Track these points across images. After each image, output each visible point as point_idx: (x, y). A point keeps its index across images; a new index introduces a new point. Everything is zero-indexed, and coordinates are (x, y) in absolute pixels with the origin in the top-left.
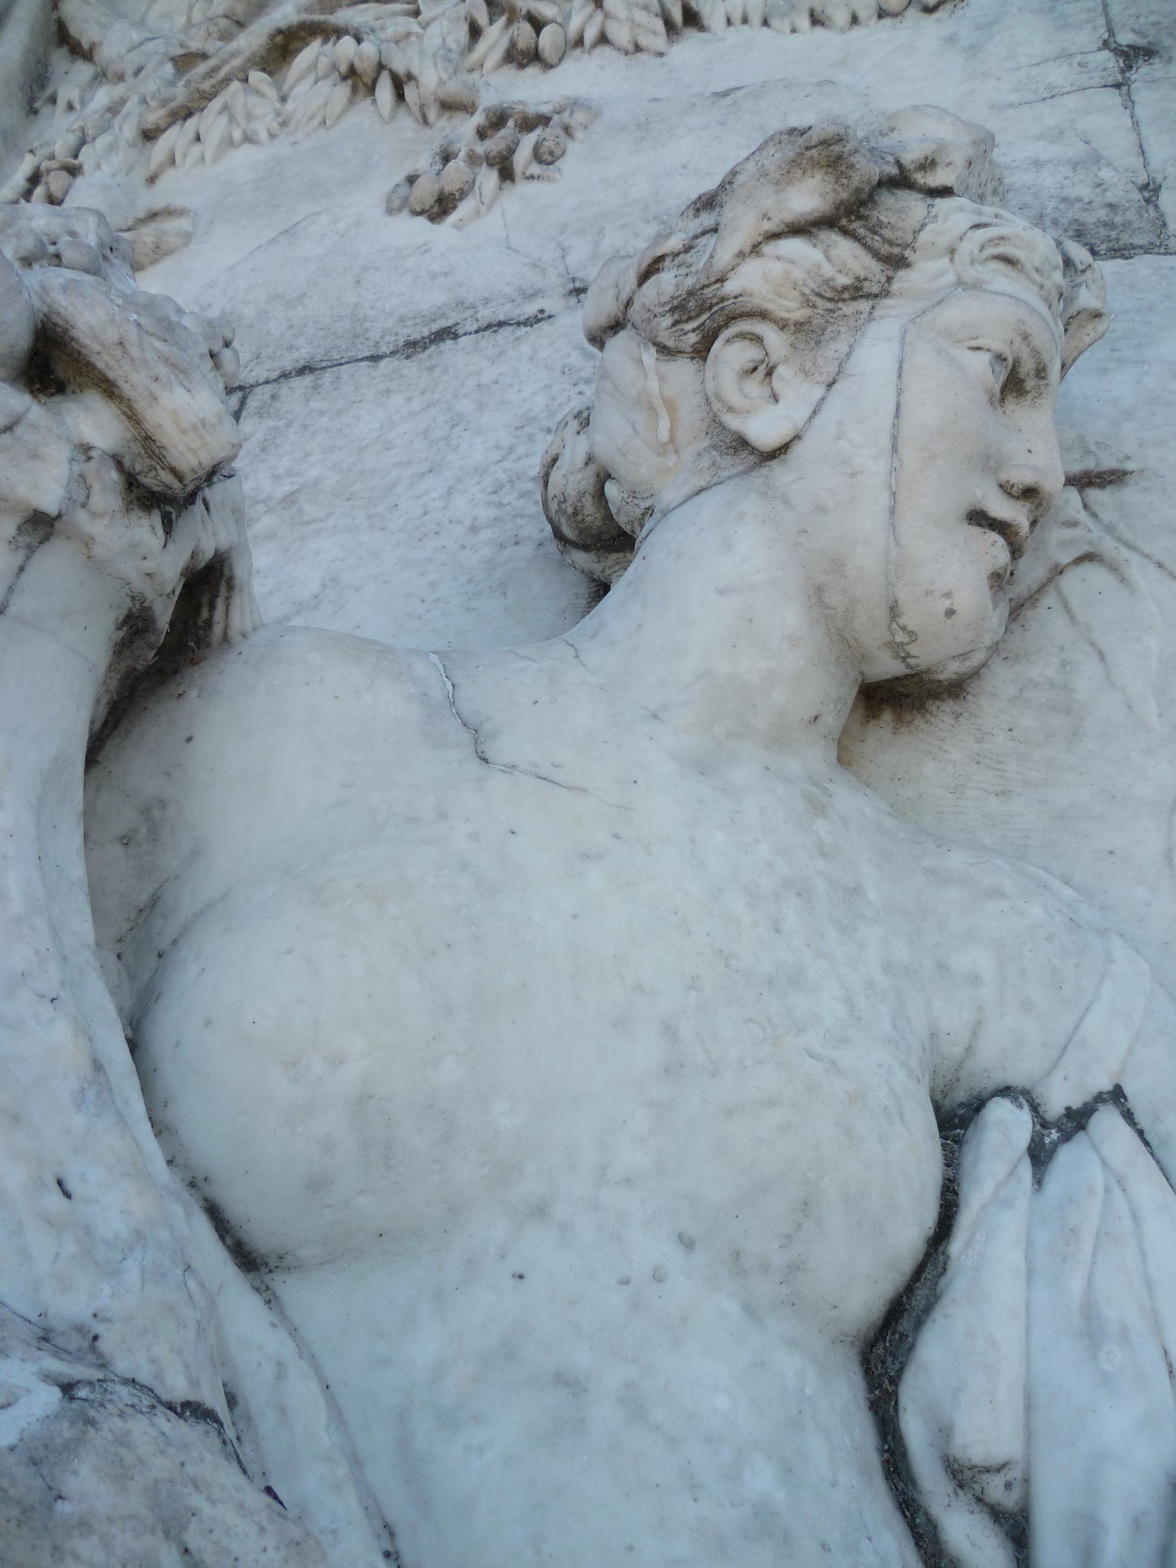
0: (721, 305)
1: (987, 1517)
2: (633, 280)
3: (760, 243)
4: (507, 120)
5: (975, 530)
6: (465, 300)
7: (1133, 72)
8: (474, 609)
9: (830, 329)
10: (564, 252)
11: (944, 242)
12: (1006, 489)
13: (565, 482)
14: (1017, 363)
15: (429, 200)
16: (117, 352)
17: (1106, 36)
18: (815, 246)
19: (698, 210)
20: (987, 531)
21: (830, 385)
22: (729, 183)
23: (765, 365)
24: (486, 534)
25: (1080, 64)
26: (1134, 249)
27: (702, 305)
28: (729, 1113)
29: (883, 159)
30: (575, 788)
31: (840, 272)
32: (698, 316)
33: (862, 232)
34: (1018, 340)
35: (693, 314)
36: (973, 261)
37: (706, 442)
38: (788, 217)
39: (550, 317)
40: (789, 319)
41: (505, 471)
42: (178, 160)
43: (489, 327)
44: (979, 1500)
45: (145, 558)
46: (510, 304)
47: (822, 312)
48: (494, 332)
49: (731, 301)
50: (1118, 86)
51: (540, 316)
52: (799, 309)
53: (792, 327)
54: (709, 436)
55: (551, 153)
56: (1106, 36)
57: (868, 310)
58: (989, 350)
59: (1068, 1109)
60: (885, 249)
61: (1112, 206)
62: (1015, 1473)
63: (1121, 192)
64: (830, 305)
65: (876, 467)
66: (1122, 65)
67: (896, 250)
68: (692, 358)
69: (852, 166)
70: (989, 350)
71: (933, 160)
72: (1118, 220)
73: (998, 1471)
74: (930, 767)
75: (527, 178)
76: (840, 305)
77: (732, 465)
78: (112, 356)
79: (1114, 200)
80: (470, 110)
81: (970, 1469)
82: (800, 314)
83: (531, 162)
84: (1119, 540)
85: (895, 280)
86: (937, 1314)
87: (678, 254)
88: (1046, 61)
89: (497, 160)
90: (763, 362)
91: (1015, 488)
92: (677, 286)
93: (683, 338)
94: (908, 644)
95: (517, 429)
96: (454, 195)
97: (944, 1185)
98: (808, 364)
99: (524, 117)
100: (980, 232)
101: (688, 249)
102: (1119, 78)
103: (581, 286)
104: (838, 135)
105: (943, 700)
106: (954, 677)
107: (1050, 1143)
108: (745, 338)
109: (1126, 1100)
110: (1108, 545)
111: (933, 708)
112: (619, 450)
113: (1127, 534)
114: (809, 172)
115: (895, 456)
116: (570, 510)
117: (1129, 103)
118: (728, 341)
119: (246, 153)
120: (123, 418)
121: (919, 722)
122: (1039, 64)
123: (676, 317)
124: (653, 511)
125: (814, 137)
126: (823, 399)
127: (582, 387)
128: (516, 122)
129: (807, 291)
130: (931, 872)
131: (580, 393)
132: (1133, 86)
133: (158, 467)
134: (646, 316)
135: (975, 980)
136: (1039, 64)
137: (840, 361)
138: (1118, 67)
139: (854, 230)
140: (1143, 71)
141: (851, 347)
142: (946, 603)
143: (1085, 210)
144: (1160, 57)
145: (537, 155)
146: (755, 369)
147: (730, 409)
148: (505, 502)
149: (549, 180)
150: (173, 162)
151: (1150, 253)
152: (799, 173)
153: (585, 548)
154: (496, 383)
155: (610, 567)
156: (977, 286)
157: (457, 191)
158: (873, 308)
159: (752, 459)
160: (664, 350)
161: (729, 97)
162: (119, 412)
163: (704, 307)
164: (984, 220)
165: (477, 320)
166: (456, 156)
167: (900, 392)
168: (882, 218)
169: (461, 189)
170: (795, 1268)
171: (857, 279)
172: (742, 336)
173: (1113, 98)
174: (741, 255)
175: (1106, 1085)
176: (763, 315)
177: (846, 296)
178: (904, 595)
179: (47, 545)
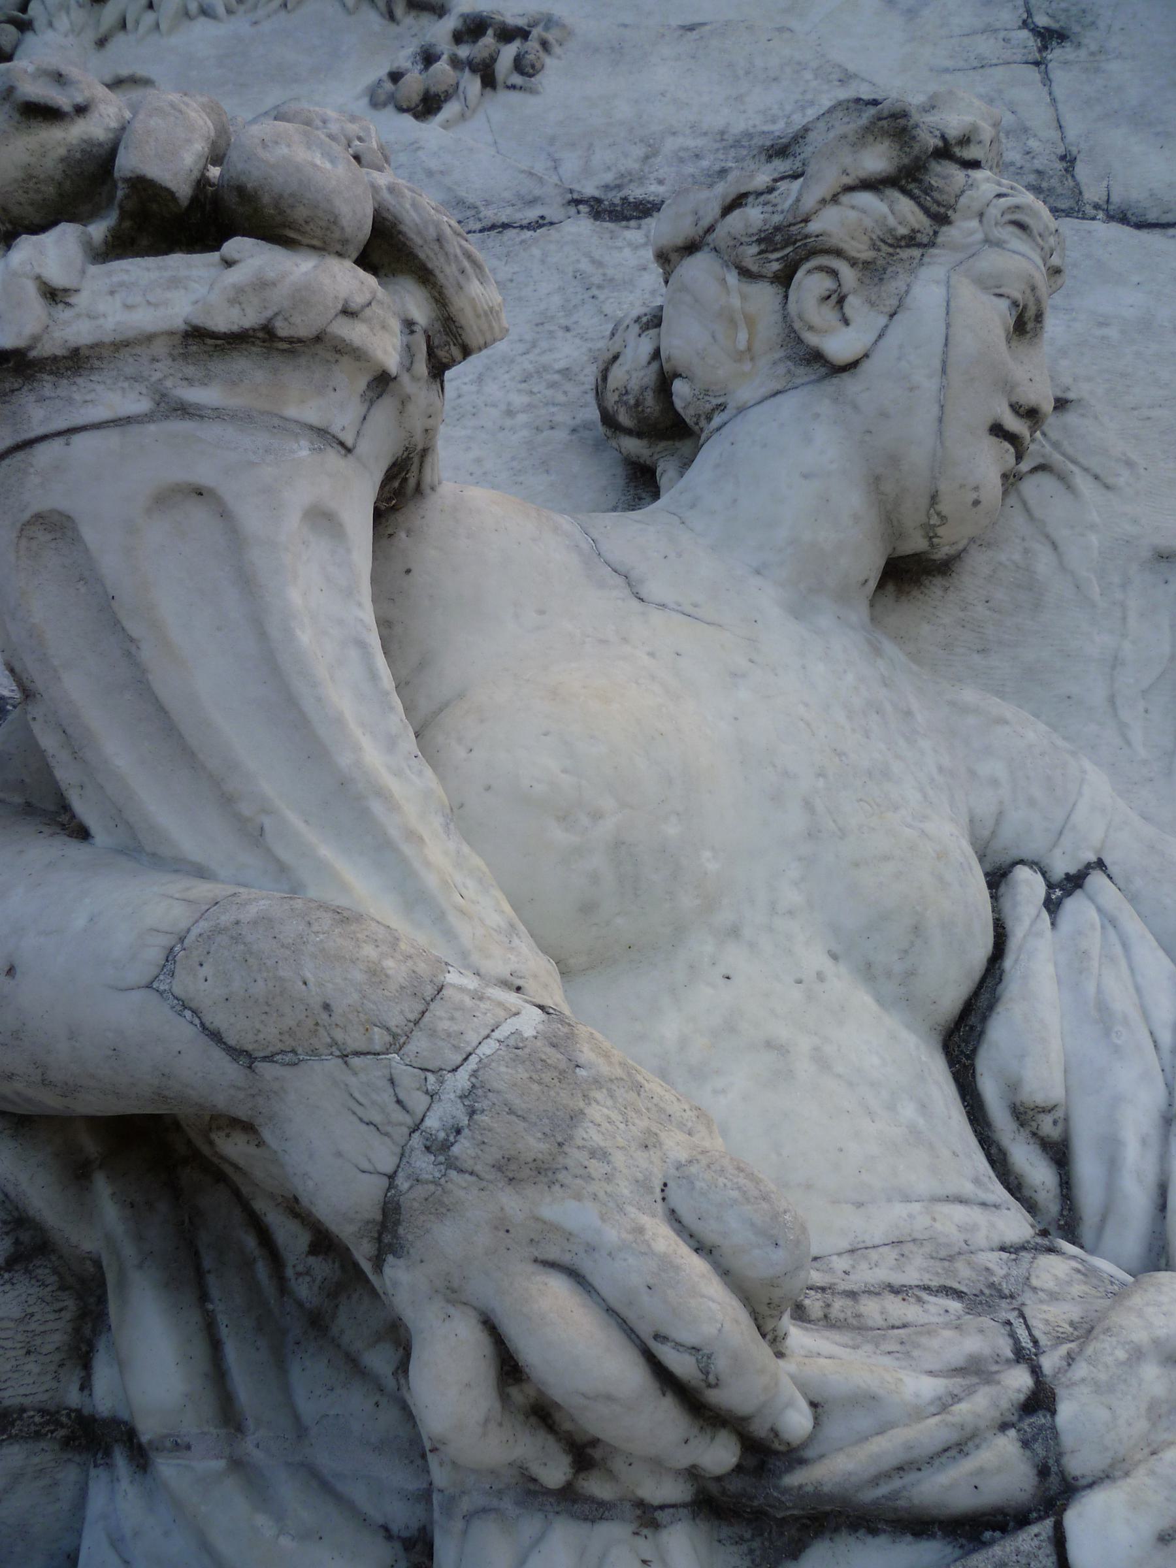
0: (805, 241)
1: (1038, 1147)
2: (717, 211)
3: (838, 194)
4: (487, 30)
5: (994, 439)
6: (465, 200)
7: (1049, 51)
8: (521, 483)
9: (890, 270)
10: (556, 165)
11: (976, 206)
12: (1015, 408)
13: (628, 377)
14: (1025, 307)
15: (416, 98)
16: (435, 247)
17: (1025, 16)
18: (882, 200)
19: (770, 157)
20: (1003, 441)
21: (892, 316)
22: (801, 137)
23: (837, 294)
24: (522, 418)
25: (1004, 40)
26: (1057, 212)
27: (788, 239)
28: (857, 865)
29: (931, 132)
30: (713, 624)
31: (900, 223)
32: (782, 248)
33: (916, 191)
34: (1028, 291)
35: (779, 246)
36: (996, 224)
37: (780, 354)
38: (862, 174)
39: (552, 224)
40: (859, 259)
41: (531, 362)
42: (129, 25)
43: (493, 227)
44: (1034, 1134)
45: (430, 416)
46: (511, 208)
47: (884, 255)
48: (499, 232)
49: (813, 239)
50: (1037, 64)
51: (541, 221)
52: (867, 250)
53: (861, 265)
54: (783, 348)
55: (533, 66)
56: (1025, 16)
57: (919, 255)
58: (1008, 297)
59: (1067, 874)
60: (934, 208)
61: (1039, 172)
62: (1059, 1114)
63: (1046, 162)
64: (891, 250)
65: (929, 385)
66: (1039, 45)
67: (942, 210)
68: (772, 283)
69: (914, 138)
70: (1008, 297)
71: (969, 137)
72: (1044, 185)
73: (1049, 1111)
74: (925, 628)
75: (508, 87)
76: (898, 250)
77: (803, 373)
78: (432, 249)
79: (1041, 168)
80: (438, 11)
81: (1032, 1110)
82: (868, 255)
83: (512, 73)
84: (1064, 454)
85: (940, 234)
86: (1000, 1008)
87: (761, 194)
88: (975, 33)
89: (481, 67)
90: (836, 291)
91: (1022, 409)
92: (765, 221)
93: (767, 265)
94: (939, 526)
95: (537, 325)
96: (440, 97)
97: (994, 923)
98: (874, 298)
99: (504, 28)
100: (1002, 200)
101: (771, 190)
102: (1038, 56)
103: (579, 198)
104: (904, 111)
105: (934, 576)
106: (945, 557)
107: (1056, 898)
108: (822, 271)
109: (1106, 869)
110: (1057, 458)
111: (927, 582)
112: (698, 354)
113: (1070, 451)
114: (879, 139)
115: (944, 377)
116: (632, 402)
117: (1047, 80)
118: (809, 272)
119: (202, 27)
120: (432, 301)
121: (916, 593)
122: (968, 35)
123: (763, 247)
124: (725, 407)
125: (885, 107)
126: (886, 326)
127: (594, 291)
128: (495, 32)
129: (874, 237)
130: (952, 704)
131: (593, 297)
132: (1050, 65)
133: (451, 343)
134: (732, 243)
135: (994, 782)
136: (968, 35)
137: (900, 296)
138: (1037, 46)
139: (911, 190)
140: (1056, 54)
141: (908, 285)
142: (974, 496)
143: (1018, 174)
144: (1071, 41)
145: (519, 65)
146: (829, 297)
147: (811, 328)
148: (535, 390)
149: (532, 91)
150: (123, 25)
151: (1071, 217)
152: (871, 138)
153: (639, 435)
154: (511, 281)
155: (659, 453)
156: (998, 244)
157: (443, 93)
158: (923, 255)
159: (823, 370)
160: (745, 274)
161: (694, 32)
162: (429, 295)
163: (788, 242)
164: (1004, 190)
165: (480, 220)
166: (438, 58)
167: (948, 326)
168: (933, 182)
169: (446, 91)
170: (911, 973)
171: (913, 230)
172: (821, 269)
173: (1034, 74)
174: (823, 202)
175: (1092, 858)
176: (838, 253)
177: (903, 243)
178: (944, 487)
179: (380, 400)
